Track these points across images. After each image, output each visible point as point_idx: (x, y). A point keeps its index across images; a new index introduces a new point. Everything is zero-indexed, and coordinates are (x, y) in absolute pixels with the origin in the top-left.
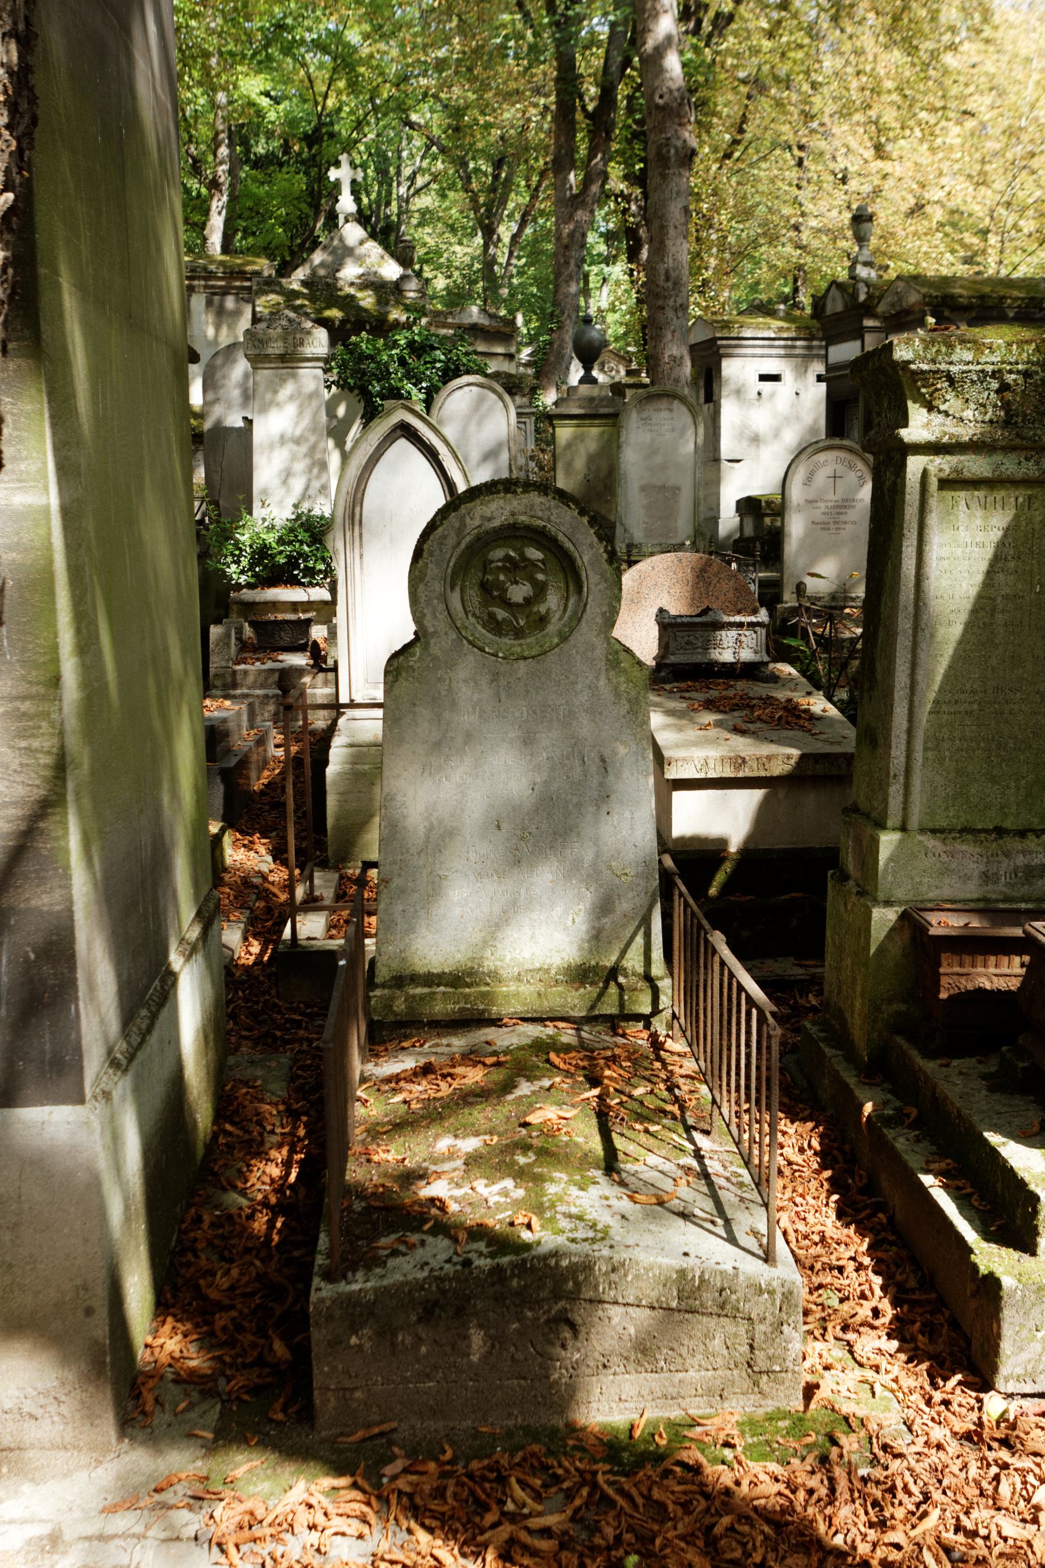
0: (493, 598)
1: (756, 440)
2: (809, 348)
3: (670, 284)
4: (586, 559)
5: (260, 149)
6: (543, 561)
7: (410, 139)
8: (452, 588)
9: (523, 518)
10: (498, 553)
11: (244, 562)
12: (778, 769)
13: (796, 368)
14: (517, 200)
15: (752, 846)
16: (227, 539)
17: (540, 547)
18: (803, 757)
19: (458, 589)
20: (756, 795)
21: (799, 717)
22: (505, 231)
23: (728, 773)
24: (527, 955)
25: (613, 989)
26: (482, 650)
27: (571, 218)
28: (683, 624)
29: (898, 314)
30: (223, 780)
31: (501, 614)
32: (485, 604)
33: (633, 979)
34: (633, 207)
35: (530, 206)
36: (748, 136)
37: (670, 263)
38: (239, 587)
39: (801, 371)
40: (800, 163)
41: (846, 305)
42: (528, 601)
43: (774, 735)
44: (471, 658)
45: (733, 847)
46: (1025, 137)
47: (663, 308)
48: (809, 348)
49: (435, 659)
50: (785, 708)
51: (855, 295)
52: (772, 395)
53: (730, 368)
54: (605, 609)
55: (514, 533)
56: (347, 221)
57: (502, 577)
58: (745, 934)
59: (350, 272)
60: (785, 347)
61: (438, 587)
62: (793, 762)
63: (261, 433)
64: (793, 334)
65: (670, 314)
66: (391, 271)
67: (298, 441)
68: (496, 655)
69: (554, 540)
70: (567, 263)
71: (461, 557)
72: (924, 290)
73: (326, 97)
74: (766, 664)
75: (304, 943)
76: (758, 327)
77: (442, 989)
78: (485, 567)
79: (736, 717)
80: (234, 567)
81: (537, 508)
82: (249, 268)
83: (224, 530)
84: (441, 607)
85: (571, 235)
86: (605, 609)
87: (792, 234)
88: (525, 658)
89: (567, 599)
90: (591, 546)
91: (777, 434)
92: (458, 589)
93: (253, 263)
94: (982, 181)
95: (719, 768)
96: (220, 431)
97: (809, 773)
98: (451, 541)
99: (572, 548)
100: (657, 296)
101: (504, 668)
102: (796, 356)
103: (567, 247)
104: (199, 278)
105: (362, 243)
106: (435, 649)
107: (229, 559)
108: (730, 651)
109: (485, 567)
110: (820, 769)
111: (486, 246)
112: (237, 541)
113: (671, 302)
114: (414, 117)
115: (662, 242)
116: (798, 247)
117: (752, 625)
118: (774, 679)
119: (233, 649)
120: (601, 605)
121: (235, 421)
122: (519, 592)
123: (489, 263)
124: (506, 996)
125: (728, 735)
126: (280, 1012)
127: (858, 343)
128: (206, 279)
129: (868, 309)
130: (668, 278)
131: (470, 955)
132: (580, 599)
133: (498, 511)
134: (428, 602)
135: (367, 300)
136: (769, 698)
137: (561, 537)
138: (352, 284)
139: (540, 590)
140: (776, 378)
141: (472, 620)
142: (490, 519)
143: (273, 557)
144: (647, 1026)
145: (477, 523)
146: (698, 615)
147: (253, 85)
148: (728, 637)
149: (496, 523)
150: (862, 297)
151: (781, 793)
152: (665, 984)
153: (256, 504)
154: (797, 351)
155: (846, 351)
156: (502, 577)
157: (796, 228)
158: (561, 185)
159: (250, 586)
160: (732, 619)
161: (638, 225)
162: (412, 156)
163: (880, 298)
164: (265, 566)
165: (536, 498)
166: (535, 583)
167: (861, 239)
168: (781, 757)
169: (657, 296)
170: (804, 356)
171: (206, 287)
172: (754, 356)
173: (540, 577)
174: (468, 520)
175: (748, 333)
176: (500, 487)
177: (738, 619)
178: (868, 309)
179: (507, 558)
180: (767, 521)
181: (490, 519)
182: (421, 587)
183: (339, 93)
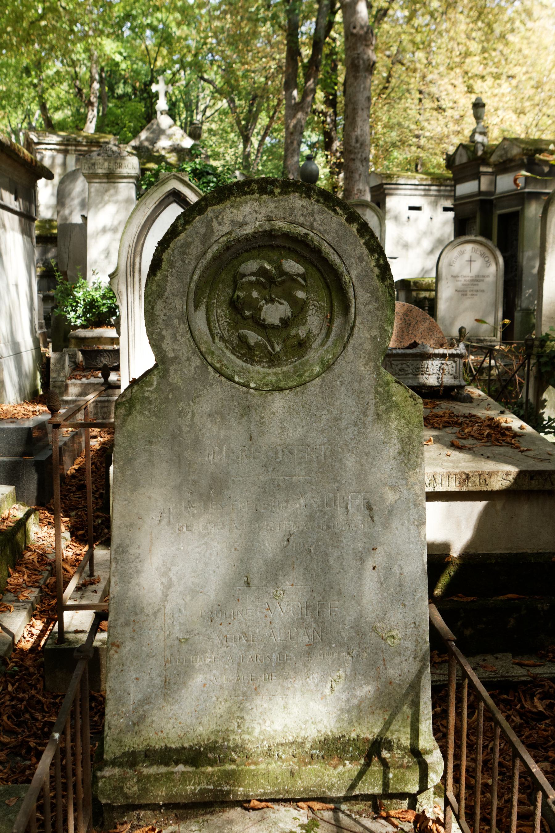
0: (244, 318)
1: (406, 246)
2: (439, 191)
3: (358, 145)
4: (354, 274)
5: (120, 90)
6: (303, 276)
7: (203, 90)
8: (196, 306)
9: (280, 224)
10: (252, 266)
11: (80, 311)
12: (498, 484)
13: (430, 203)
14: (263, 120)
15: (472, 551)
16: (68, 295)
17: (300, 259)
18: (520, 474)
19: (203, 307)
20: (479, 506)
21: (504, 434)
22: (255, 141)
23: (453, 487)
24: (278, 727)
25: (376, 767)
26: (231, 379)
27: (294, 116)
28: (397, 355)
29: (505, 162)
30: (37, 471)
31: (253, 337)
32: (235, 325)
33: (398, 753)
34: (329, 120)
35: (268, 127)
36: (392, 85)
37: (358, 132)
38: (76, 327)
39: (435, 204)
40: (420, 100)
41: (469, 158)
42: (285, 323)
43: (484, 450)
44: (218, 389)
45: (455, 552)
46: (547, 88)
47: (354, 160)
48: (439, 191)
49: (174, 388)
50: (489, 426)
51: (475, 151)
52: (416, 220)
53: (391, 202)
54: (375, 333)
55: (269, 241)
56: (162, 114)
57: (255, 294)
58: (468, 632)
59: (163, 143)
60: (424, 190)
61: (179, 304)
62: (511, 478)
63: (91, 227)
64: (429, 182)
65: (358, 164)
66: (188, 143)
67: (114, 230)
68: (248, 386)
69: (317, 251)
70: (292, 143)
71: (207, 268)
72: (523, 146)
73: (156, 60)
74: (461, 387)
75: (71, 636)
76: (408, 178)
77: (181, 768)
78: (235, 282)
79: (450, 433)
80: (72, 314)
81: (298, 213)
82: (102, 140)
83: (66, 289)
84: (183, 328)
85: (295, 127)
86: (375, 333)
87: (415, 140)
88: (281, 389)
89: (331, 321)
90: (361, 259)
91: (419, 242)
92: (203, 307)
93: (105, 137)
94: (521, 112)
95: (445, 483)
96: (67, 228)
97: (525, 488)
98: (195, 250)
99: (338, 261)
100: (350, 152)
101: (256, 399)
102: (431, 196)
103: (292, 134)
104: (71, 145)
105: (170, 127)
106: (175, 378)
107: (69, 309)
108: (435, 377)
109: (235, 282)
110: (535, 484)
111: (245, 147)
112: (75, 297)
113: (359, 156)
114: (206, 76)
115: (354, 119)
116: (419, 147)
117: (452, 356)
118: (469, 399)
119: (67, 369)
120: (370, 328)
121: (77, 219)
122: (274, 313)
123: (246, 157)
124: (254, 775)
125: (449, 452)
126: (42, 711)
127: (476, 182)
128: (76, 146)
129: (484, 160)
130: (357, 141)
131: (213, 727)
132: (346, 321)
133: (250, 215)
134: (168, 323)
135: (172, 158)
136: (472, 416)
137: (325, 248)
138: (164, 148)
139: (300, 309)
140: (418, 209)
141: (220, 344)
142: (242, 225)
143: (99, 307)
144: (412, 806)
145: (226, 228)
146: (408, 348)
147: (110, 47)
148: (433, 365)
149: (249, 230)
150: (480, 153)
151: (499, 505)
152: (435, 758)
153: (89, 273)
154: (432, 193)
155: (466, 188)
156: (255, 294)
157: (418, 137)
158: (289, 97)
159: (83, 327)
160: (436, 351)
161: (331, 129)
162: (204, 98)
163: (492, 153)
164: (94, 314)
165: (297, 201)
166: (293, 302)
167: (478, 117)
168: (502, 474)
169: (350, 152)
170: (436, 196)
171: (76, 150)
172: (405, 195)
173: (300, 294)
174: (215, 225)
175: (401, 181)
176: (255, 186)
177: (441, 351)
178: (484, 160)
179: (262, 272)
180: (414, 294)
181: (242, 225)
182: (159, 304)
183: (164, 58)
